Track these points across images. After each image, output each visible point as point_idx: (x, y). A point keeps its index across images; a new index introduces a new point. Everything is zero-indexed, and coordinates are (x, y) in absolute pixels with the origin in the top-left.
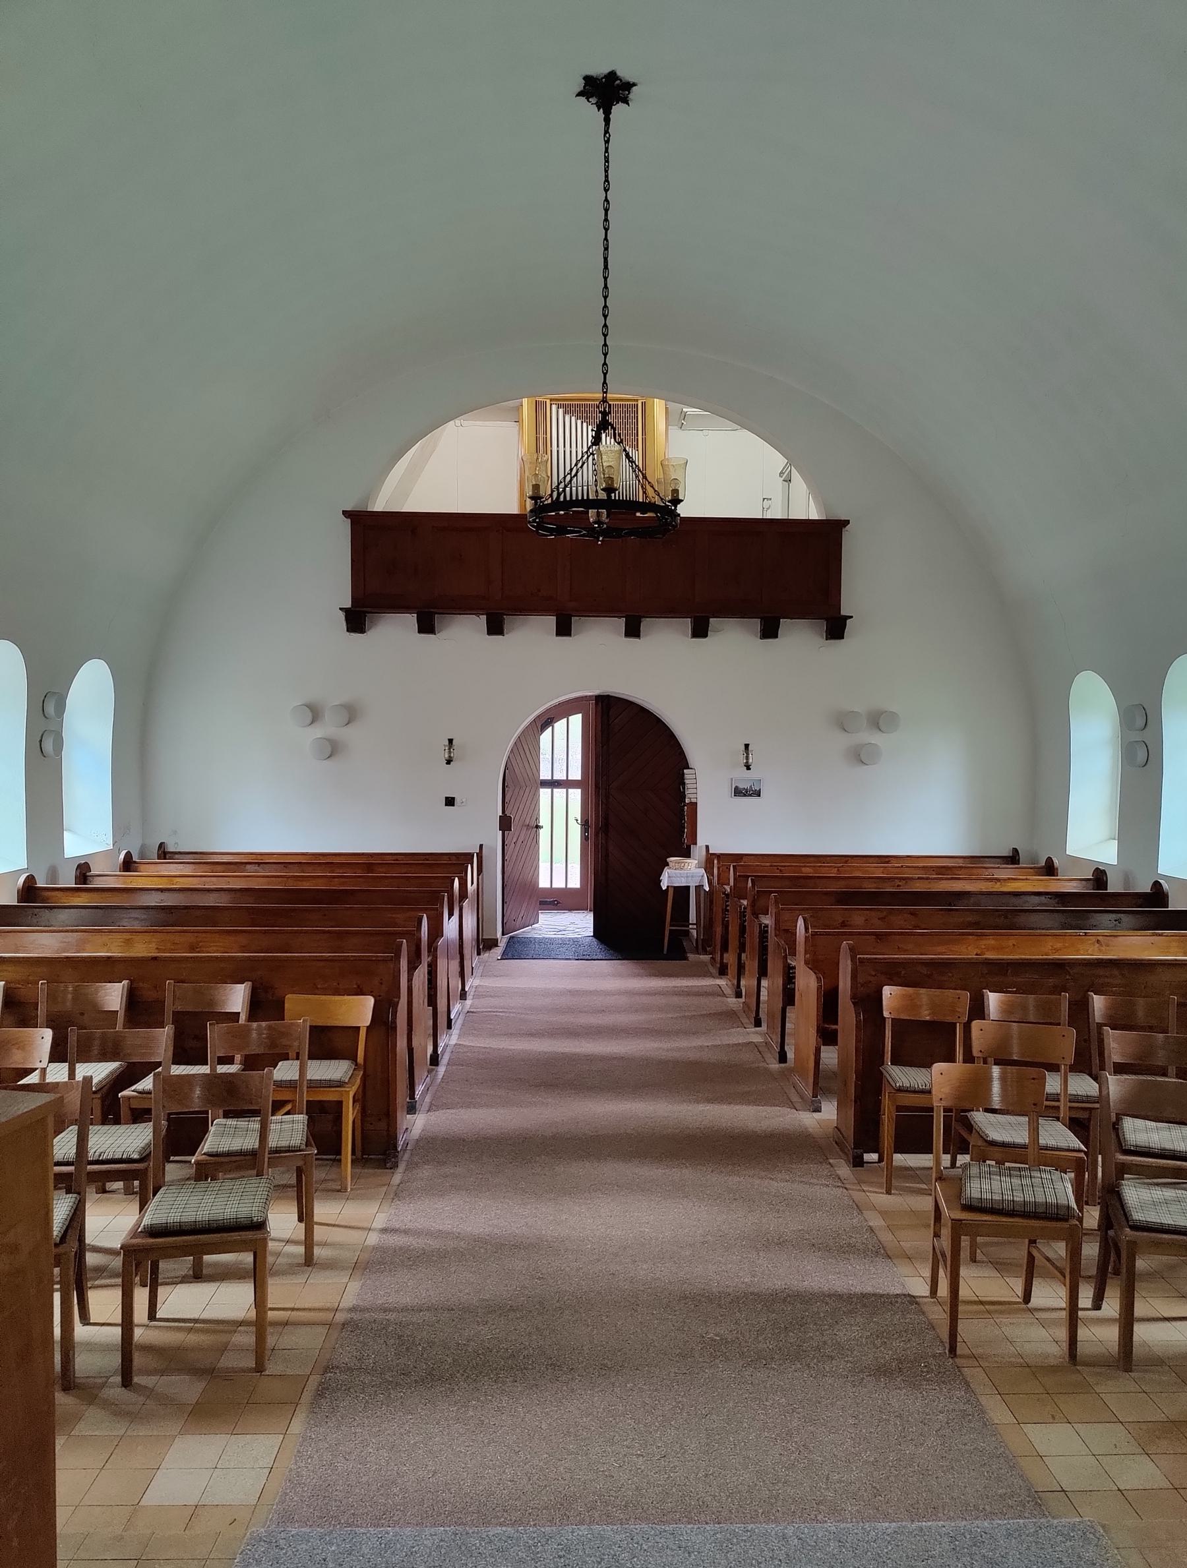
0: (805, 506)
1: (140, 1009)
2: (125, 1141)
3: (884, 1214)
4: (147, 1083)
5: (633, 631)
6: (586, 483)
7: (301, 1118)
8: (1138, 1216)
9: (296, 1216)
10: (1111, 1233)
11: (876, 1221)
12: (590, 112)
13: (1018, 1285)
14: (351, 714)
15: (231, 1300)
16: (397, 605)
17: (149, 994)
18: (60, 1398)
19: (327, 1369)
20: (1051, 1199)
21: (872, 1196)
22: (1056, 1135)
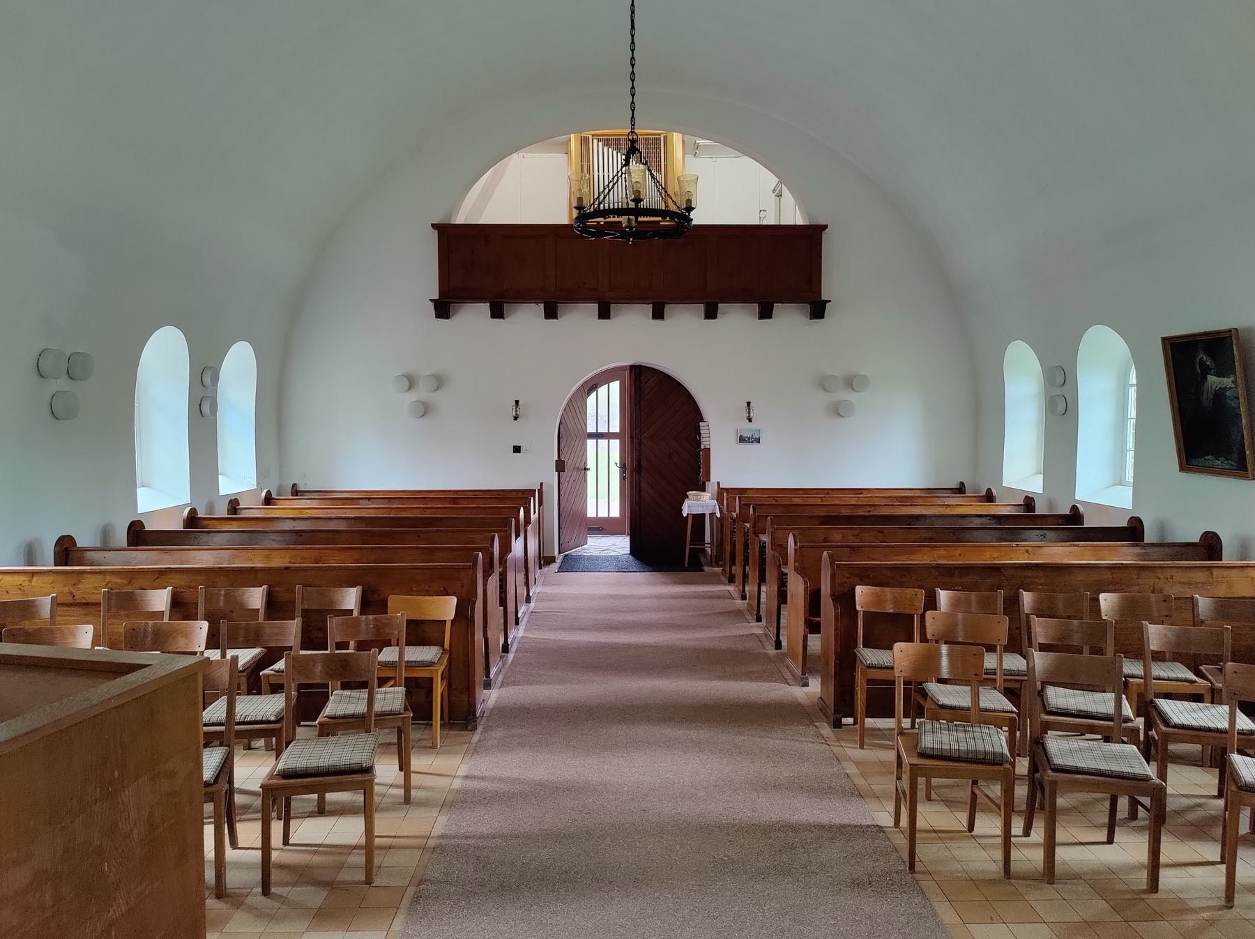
0: (792, 215)
1: (275, 607)
2: (267, 707)
3: (857, 764)
4: (280, 665)
5: (658, 314)
6: (619, 197)
7: (400, 690)
8: (1058, 761)
9: (397, 767)
10: (1037, 775)
11: (852, 769)
13: (963, 818)
14: (439, 382)
15: (348, 830)
16: (473, 296)
17: (283, 596)
18: (211, 903)
19: (421, 882)
20: (989, 748)
22: (994, 700)
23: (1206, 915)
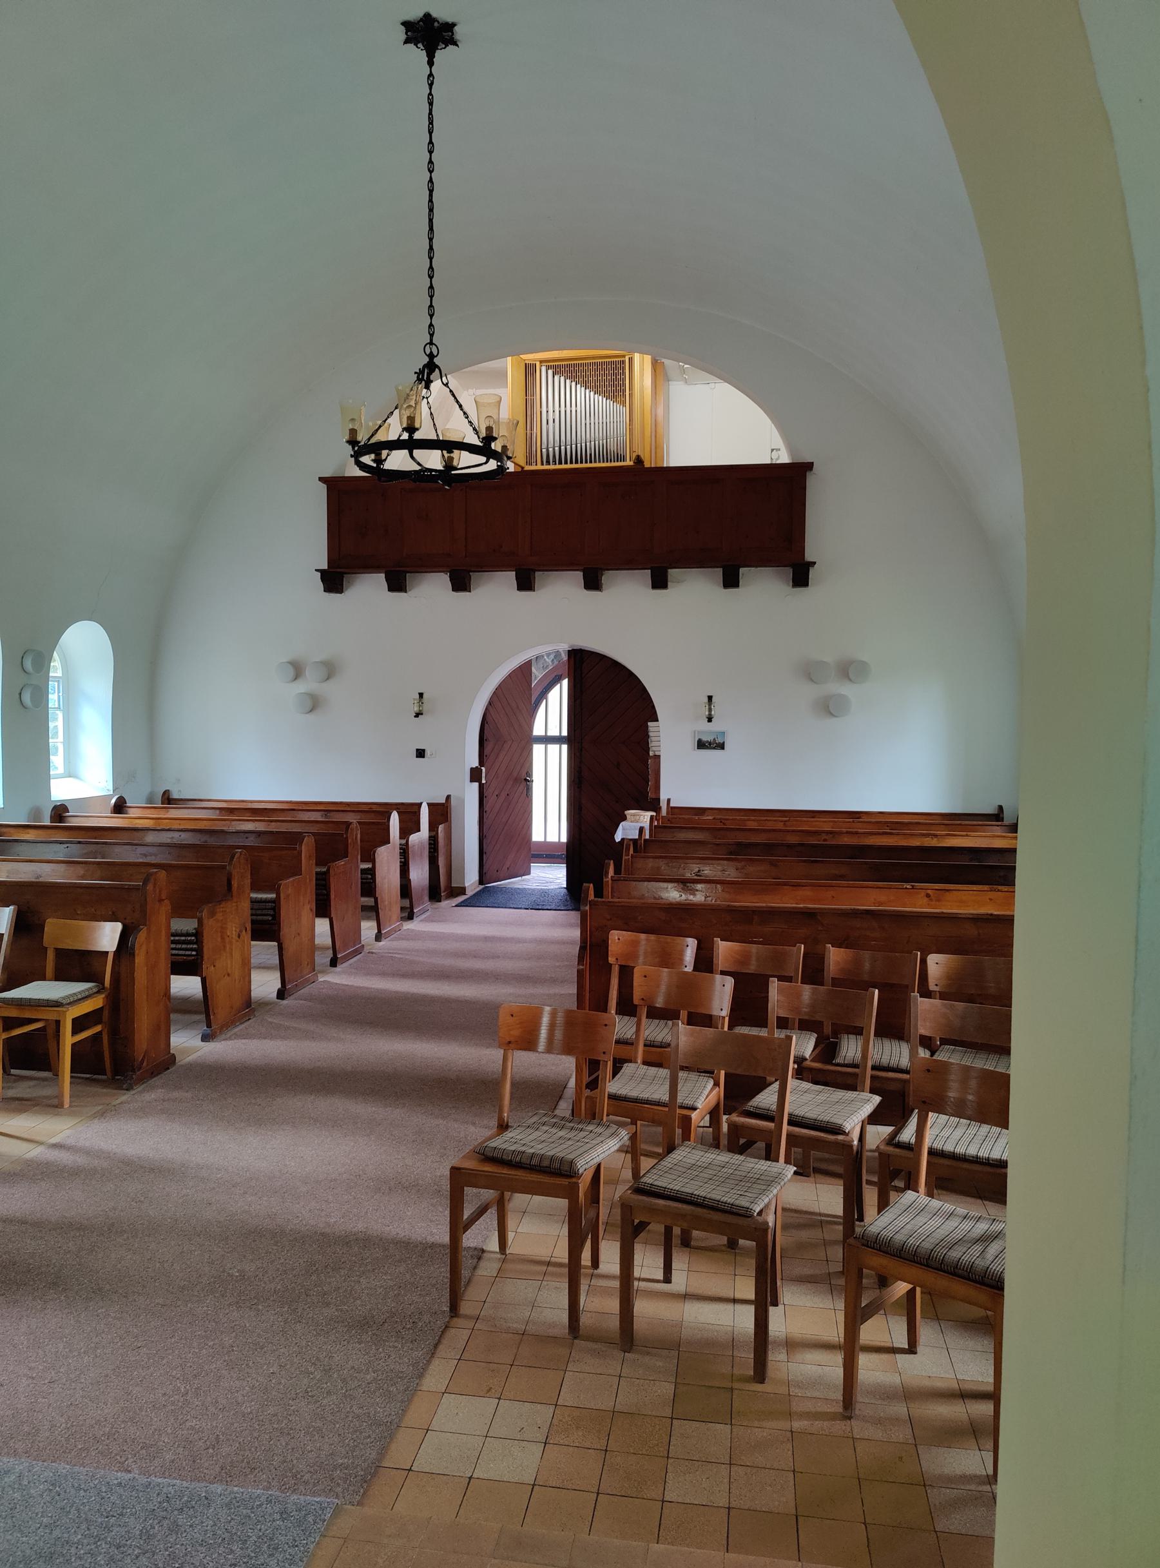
12: (418, 54)
14: (330, 670)
16: (367, 566)
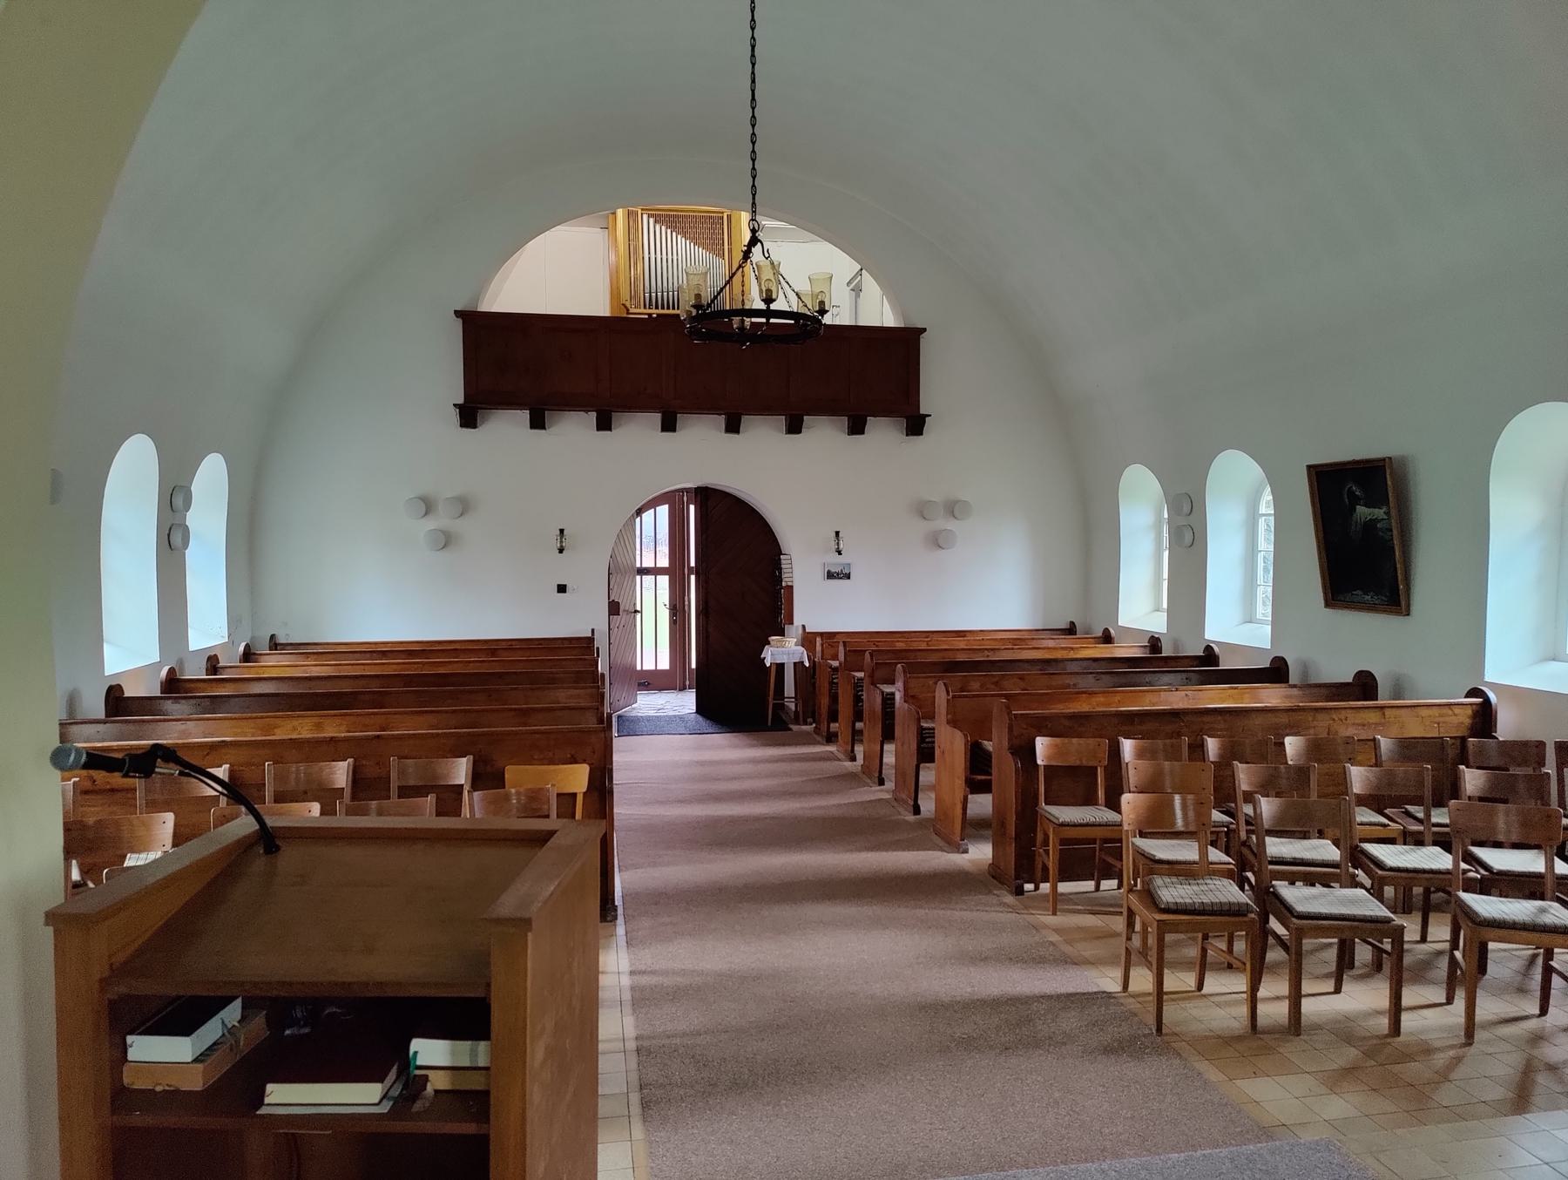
3: (1057, 931)
14: (464, 506)
16: (508, 401)
21: (1043, 918)
23: (1452, 1053)
